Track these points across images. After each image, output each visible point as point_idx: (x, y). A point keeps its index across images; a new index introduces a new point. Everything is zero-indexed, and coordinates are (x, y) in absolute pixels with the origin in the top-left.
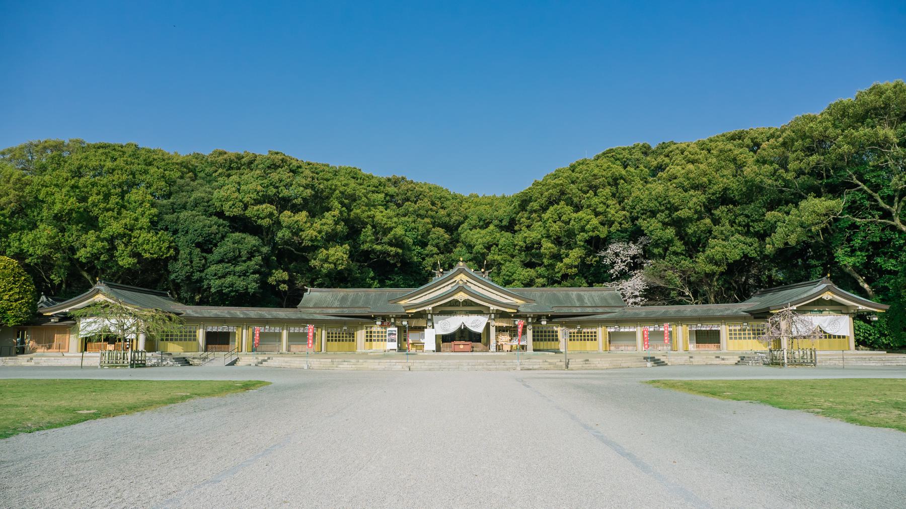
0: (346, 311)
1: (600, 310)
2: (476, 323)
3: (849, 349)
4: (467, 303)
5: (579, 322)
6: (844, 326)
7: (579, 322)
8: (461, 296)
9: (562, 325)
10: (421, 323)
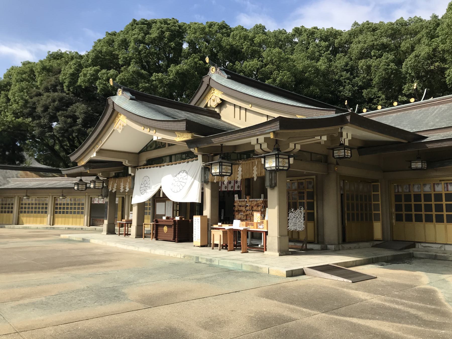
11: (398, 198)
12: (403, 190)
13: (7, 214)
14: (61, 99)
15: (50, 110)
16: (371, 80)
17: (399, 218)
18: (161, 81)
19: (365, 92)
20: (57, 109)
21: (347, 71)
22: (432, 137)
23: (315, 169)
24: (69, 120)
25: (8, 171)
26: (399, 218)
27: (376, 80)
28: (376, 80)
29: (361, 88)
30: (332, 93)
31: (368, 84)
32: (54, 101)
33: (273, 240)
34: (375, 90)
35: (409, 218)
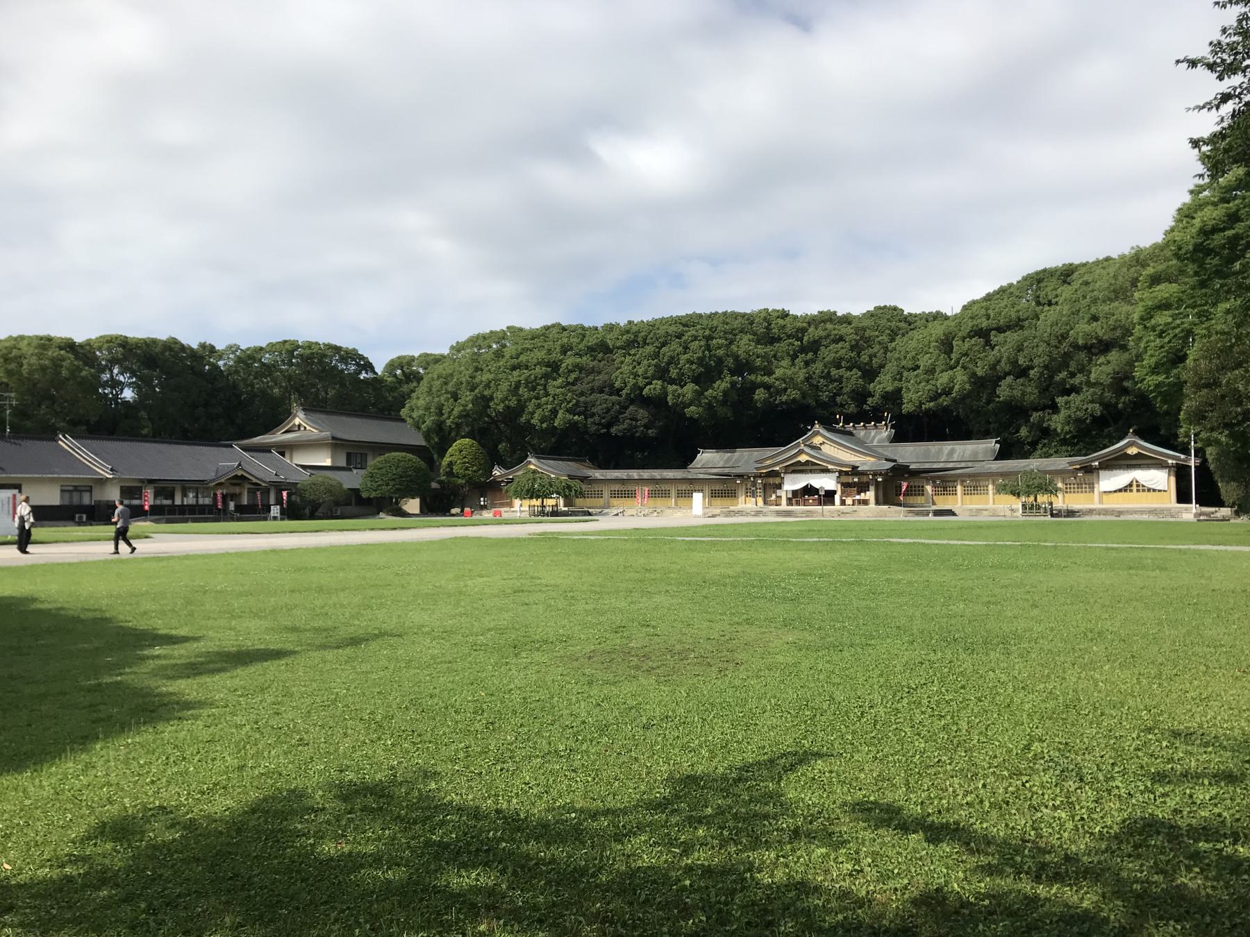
0: (726, 471)
1: (963, 465)
2: (826, 482)
4: (1138, 456)
5: (939, 477)
6: (1160, 479)
8: (803, 458)
9: (927, 479)
10: (777, 481)
14: (619, 403)
19: (838, 399)
28: (845, 390)
29: (835, 395)
33: (872, 500)
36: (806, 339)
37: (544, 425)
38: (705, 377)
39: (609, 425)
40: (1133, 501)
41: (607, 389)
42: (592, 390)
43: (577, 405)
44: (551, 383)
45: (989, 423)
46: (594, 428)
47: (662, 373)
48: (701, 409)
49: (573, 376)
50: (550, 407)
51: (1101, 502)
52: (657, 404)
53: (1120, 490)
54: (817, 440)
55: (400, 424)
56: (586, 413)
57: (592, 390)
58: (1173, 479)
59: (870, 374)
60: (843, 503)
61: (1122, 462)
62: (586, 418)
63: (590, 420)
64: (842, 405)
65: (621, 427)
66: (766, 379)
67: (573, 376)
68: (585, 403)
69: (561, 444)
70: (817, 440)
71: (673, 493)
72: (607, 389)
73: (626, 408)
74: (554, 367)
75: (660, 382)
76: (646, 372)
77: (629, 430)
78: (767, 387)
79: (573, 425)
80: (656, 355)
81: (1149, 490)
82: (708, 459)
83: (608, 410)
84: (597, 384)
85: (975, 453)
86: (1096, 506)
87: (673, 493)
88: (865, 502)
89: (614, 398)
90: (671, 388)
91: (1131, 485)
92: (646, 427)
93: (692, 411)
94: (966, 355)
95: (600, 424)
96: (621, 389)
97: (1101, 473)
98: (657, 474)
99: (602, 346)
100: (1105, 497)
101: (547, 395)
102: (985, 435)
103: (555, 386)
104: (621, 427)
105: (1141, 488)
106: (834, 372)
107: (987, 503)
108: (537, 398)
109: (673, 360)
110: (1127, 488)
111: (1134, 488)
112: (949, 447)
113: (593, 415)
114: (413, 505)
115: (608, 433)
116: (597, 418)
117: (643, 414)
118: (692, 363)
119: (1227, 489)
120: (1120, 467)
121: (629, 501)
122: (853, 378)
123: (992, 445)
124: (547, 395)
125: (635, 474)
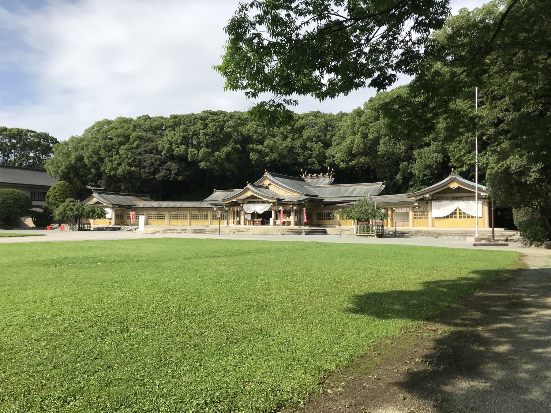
3: (427, 226)
4: (459, 190)
7: (341, 207)
11: (318, 213)
12: (319, 211)
13: (418, 219)
14: (160, 160)
15: (154, 165)
16: (312, 154)
17: (318, 219)
18: (220, 157)
19: (309, 160)
20: (160, 165)
21: (301, 148)
22: (326, 200)
23: (300, 207)
24: (168, 172)
25: (17, 183)
26: (318, 219)
27: (314, 155)
28: (314, 155)
29: (308, 158)
30: (294, 159)
31: (310, 157)
32: (156, 160)
33: (292, 223)
34: (314, 159)
35: (320, 219)
36: (296, 125)
37: (112, 173)
38: (216, 144)
39: (154, 174)
40: (456, 225)
41: (154, 151)
42: (146, 152)
43: (135, 160)
44: (123, 147)
45: (385, 172)
46: (144, 175)
47: (185, 141)
48: (208, 164)
49: (136, 143)
50: (116, 165)
51: (433, 225)
52: (182, 159)
53: (447, 217)
54: (266, 182)
55: (43, 173)
56: (140, 165)
57: (146, 152)
58: (486, 208)
59: (327, 145)
60: (275, 224)
61: (446, 195)
62: (140, 169)
63: (142, 170)
64: (311, 165)
65: (160, 175)
66: (259, 147)
67: (136, 143)
68: (140, 159)
69: (114, 185)
70: (266, 182)
71: (188, 216)
72: (154, 151)
73: (165, 163)
74: (127, 137)
75: (184, 147)
76: (177, 140)
77: (165, 177)
78: (259, 152)
79: (130, 173)
80: (186, 130)
81: (468, 217)
82: (219, 195)
83: (152, 164)
84: (148, 148)
85: (367, 191)
86: (430, 228)
87: (188, 216)
88: (289, 223)
89: (158, 157)
90: (190, 150)
91: (455, 212)
92: (177, 174)
93: (202, 164)
94: (364, 125)
95: (148, 173)
96: (161, 152)
97: (434, 203)
98: (178, 204)
99: (156, 127)
100: (436, 221)
101: (118, 154)
102: (376, 180)
103: (123, 150)
104: (160, 175)
105: (463, 215)
106: (308, 144)
107: (409, 225)
108: (110, 156)
109: (196, 134)
110: (452, 215)
111: (458, 215)
112: (353, 188)
113: (144, 168)
114: (29, 222)
115: (154, 179)
116: (147, 169)
117: (174, 166)
118: (207, 135)
119: (519, 215)
120: (447, 199)
121: (160, 221)
122: (317, 147)
123: (380, 186)
124: (118, 154)
125: (165, 204)
